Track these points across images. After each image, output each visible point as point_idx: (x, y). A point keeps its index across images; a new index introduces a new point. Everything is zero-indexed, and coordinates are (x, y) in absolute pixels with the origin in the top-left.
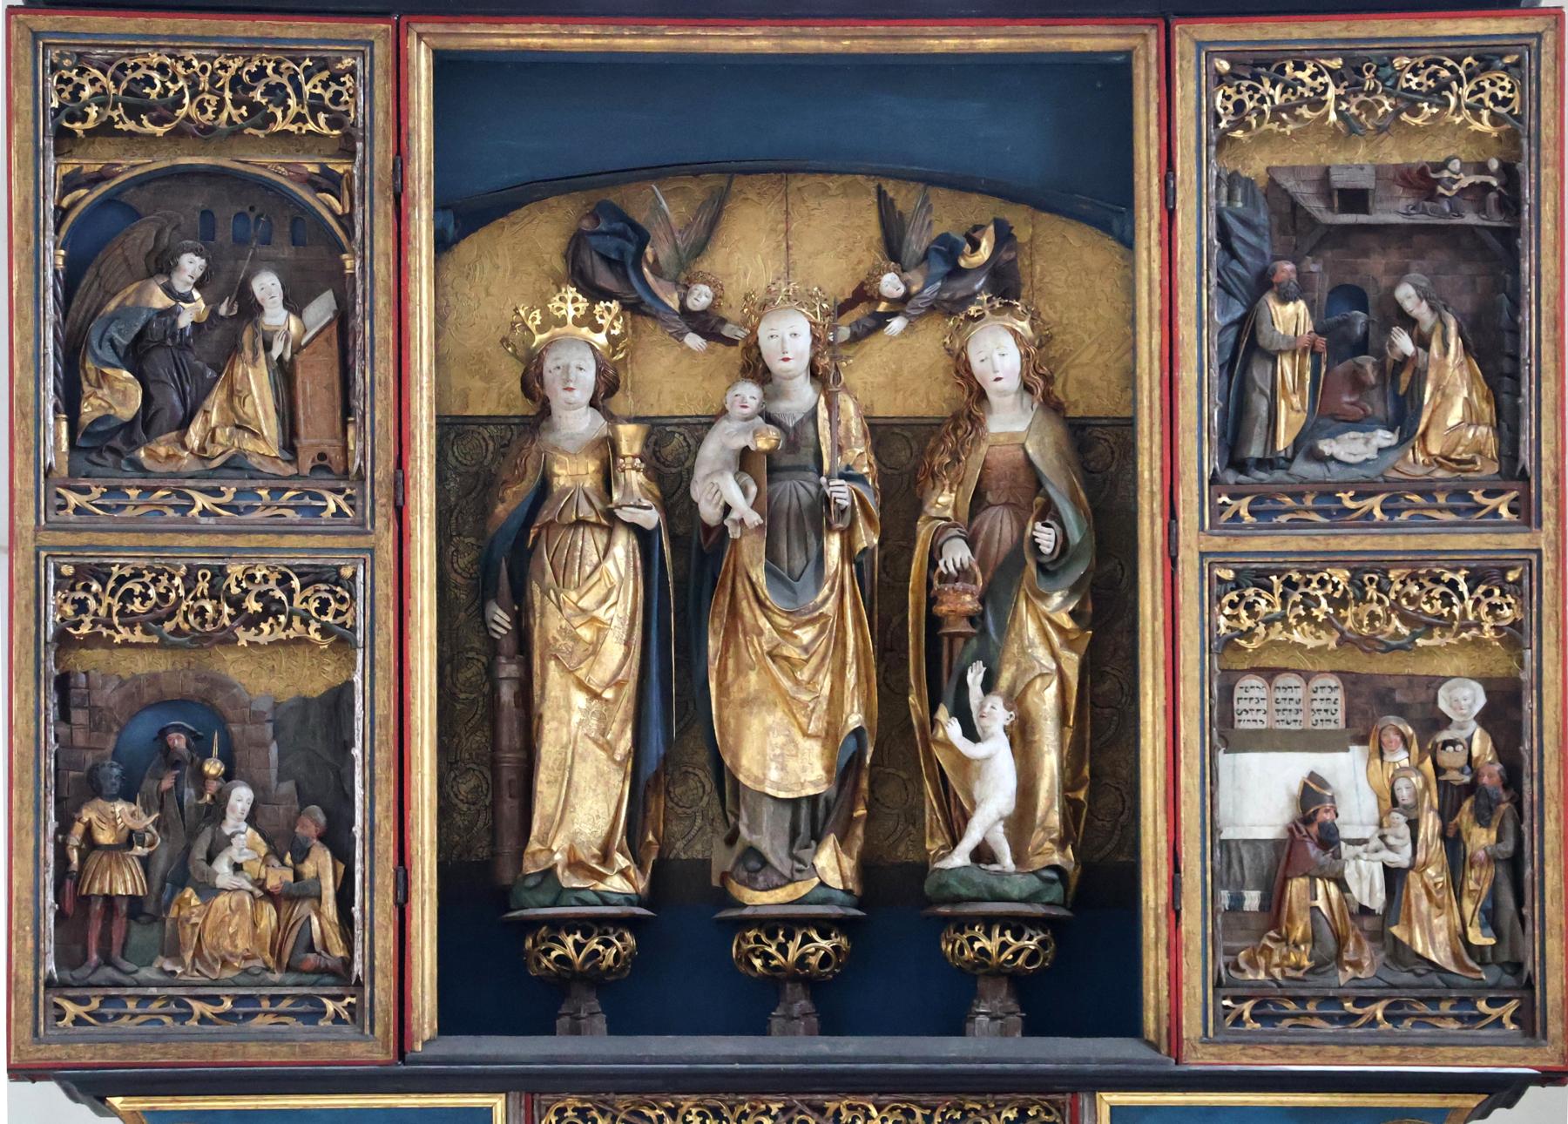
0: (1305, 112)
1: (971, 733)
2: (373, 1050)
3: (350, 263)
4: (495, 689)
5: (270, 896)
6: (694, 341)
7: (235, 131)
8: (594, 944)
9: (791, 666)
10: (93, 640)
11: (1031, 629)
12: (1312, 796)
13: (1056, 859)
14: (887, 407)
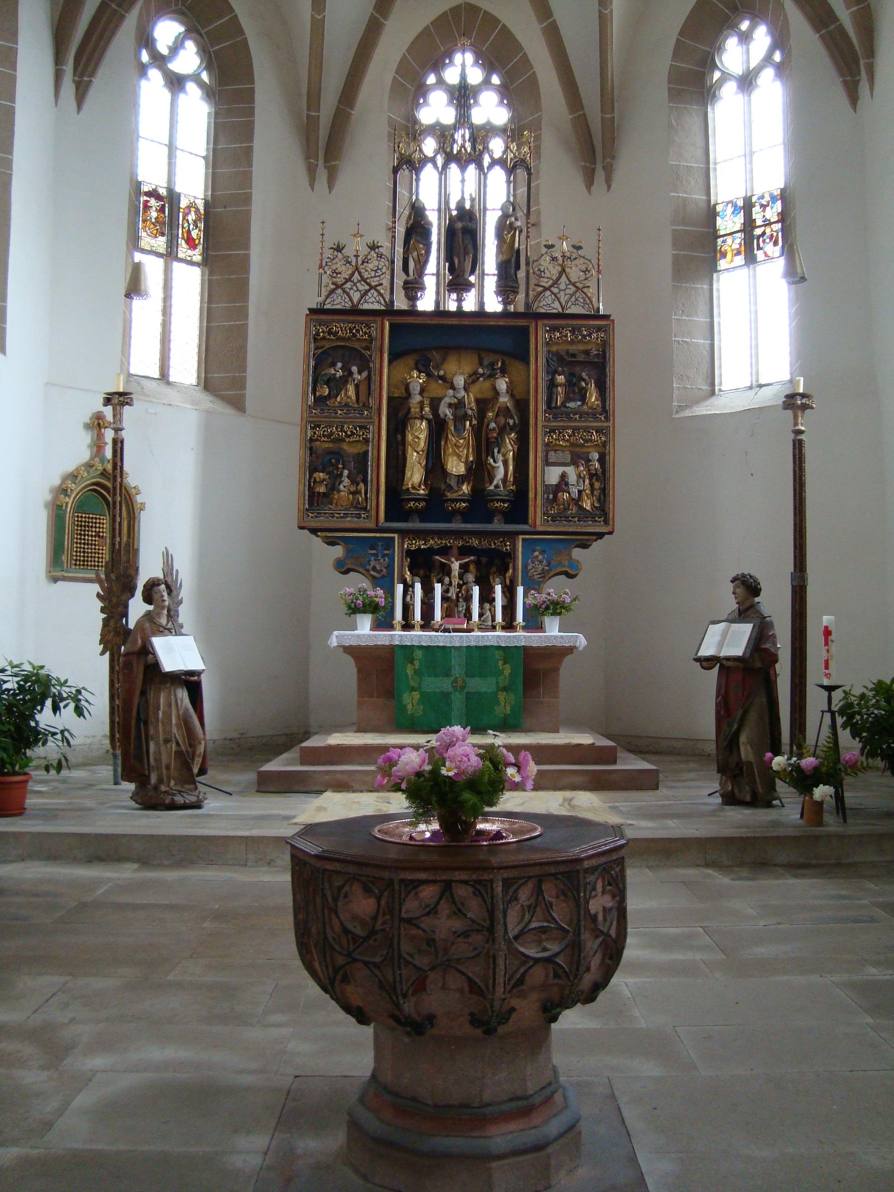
0: (564, 338)
1: (495, 461)
2: (371, 525)
3: (371, 365)
4: (398, 452)
5: (351, 493)
6: (440, 382)
7: (349, 338)
8: (417, 504)
9: (458, 447)
10: (317, 440)
11: (507, 441)
12: (563, 476)
13: (512, 488)
14: (479, 396)
